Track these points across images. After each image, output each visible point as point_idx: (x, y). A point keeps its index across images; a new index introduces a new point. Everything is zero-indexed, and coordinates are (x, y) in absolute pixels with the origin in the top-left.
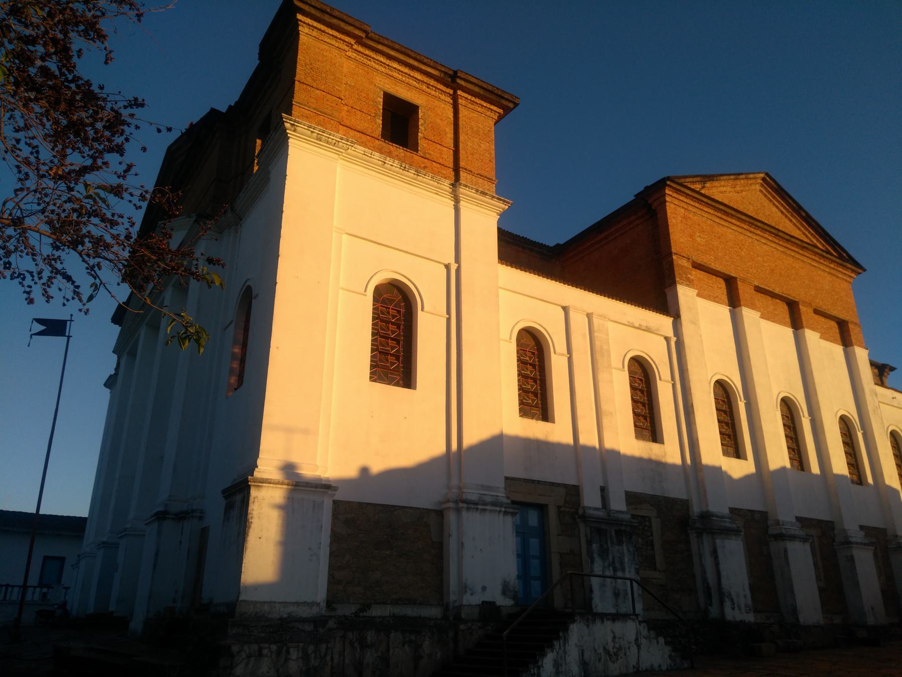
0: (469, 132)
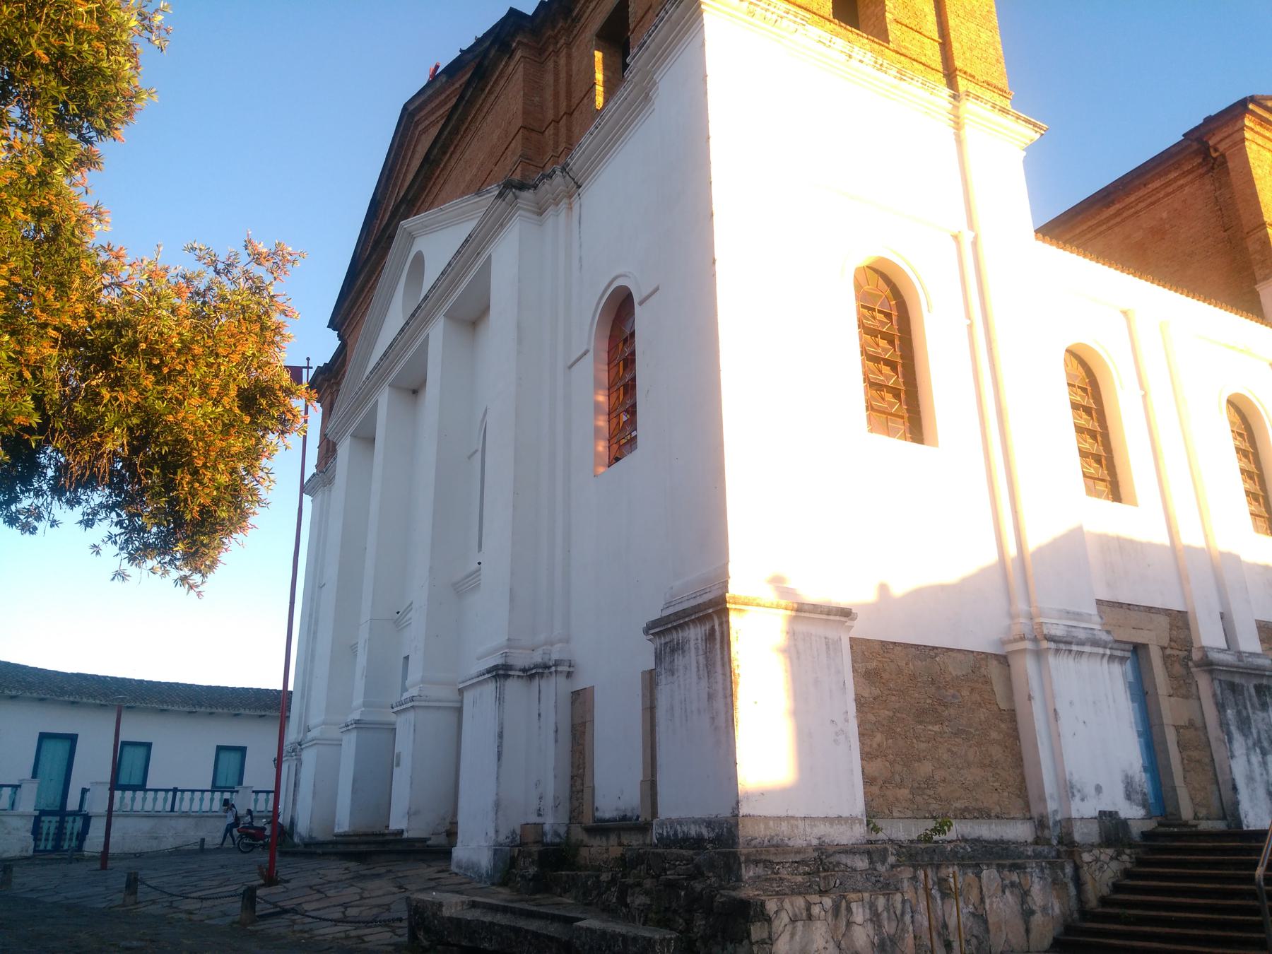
0: (961, 13)
